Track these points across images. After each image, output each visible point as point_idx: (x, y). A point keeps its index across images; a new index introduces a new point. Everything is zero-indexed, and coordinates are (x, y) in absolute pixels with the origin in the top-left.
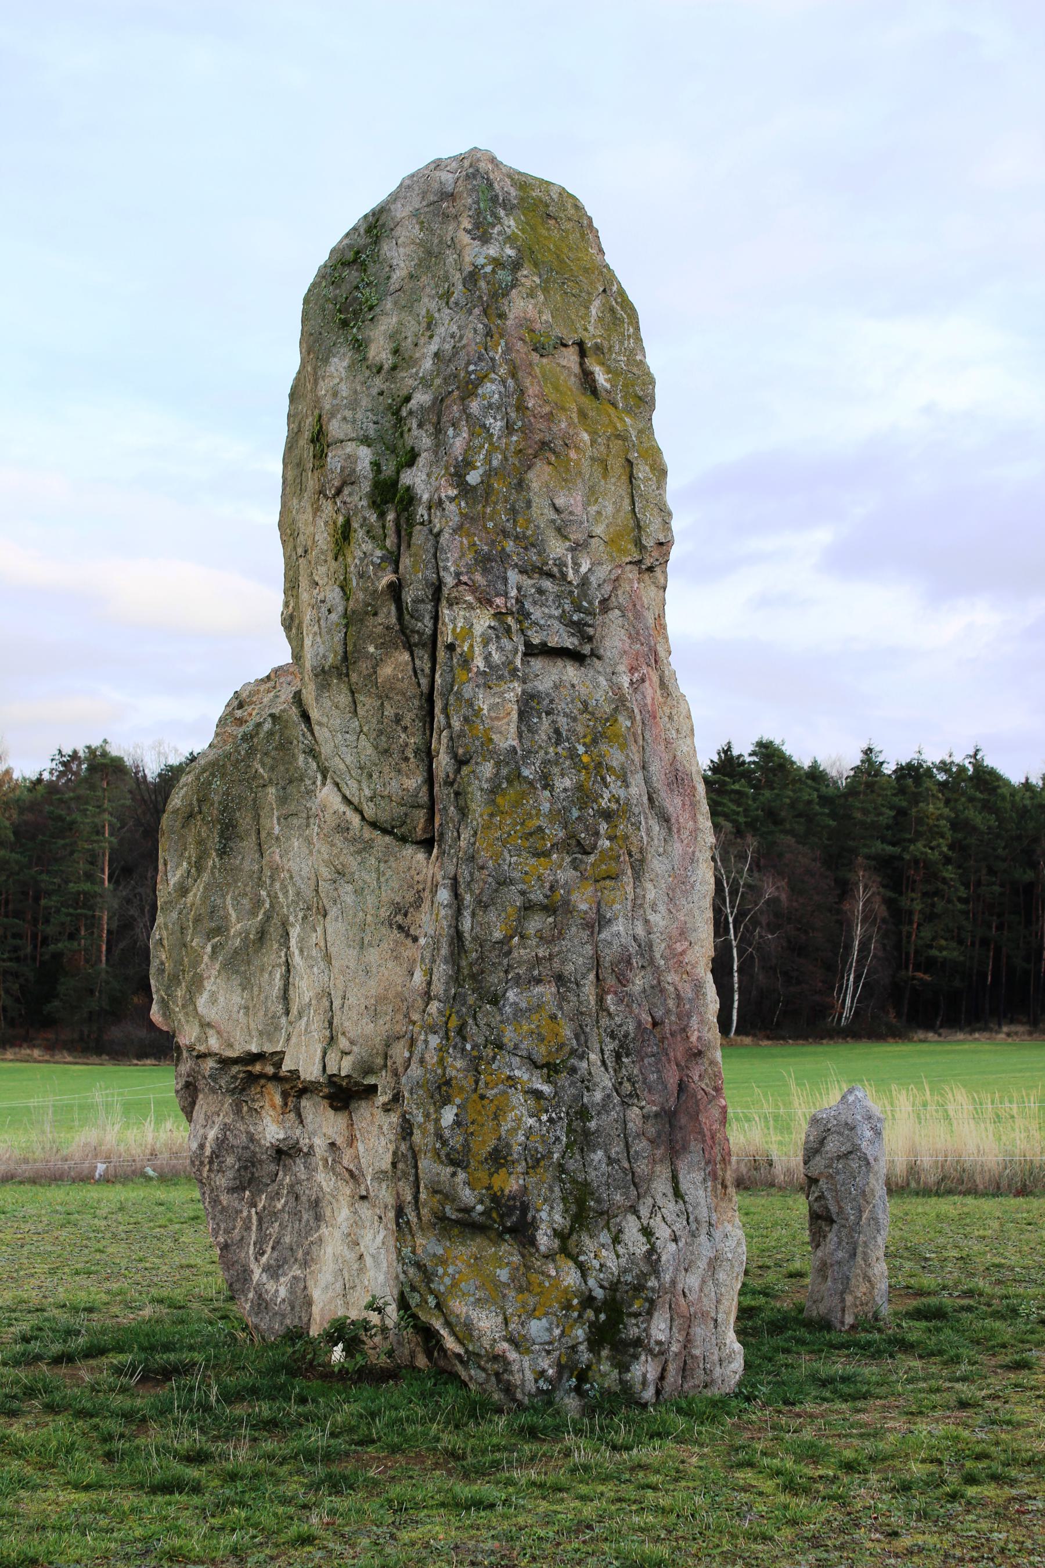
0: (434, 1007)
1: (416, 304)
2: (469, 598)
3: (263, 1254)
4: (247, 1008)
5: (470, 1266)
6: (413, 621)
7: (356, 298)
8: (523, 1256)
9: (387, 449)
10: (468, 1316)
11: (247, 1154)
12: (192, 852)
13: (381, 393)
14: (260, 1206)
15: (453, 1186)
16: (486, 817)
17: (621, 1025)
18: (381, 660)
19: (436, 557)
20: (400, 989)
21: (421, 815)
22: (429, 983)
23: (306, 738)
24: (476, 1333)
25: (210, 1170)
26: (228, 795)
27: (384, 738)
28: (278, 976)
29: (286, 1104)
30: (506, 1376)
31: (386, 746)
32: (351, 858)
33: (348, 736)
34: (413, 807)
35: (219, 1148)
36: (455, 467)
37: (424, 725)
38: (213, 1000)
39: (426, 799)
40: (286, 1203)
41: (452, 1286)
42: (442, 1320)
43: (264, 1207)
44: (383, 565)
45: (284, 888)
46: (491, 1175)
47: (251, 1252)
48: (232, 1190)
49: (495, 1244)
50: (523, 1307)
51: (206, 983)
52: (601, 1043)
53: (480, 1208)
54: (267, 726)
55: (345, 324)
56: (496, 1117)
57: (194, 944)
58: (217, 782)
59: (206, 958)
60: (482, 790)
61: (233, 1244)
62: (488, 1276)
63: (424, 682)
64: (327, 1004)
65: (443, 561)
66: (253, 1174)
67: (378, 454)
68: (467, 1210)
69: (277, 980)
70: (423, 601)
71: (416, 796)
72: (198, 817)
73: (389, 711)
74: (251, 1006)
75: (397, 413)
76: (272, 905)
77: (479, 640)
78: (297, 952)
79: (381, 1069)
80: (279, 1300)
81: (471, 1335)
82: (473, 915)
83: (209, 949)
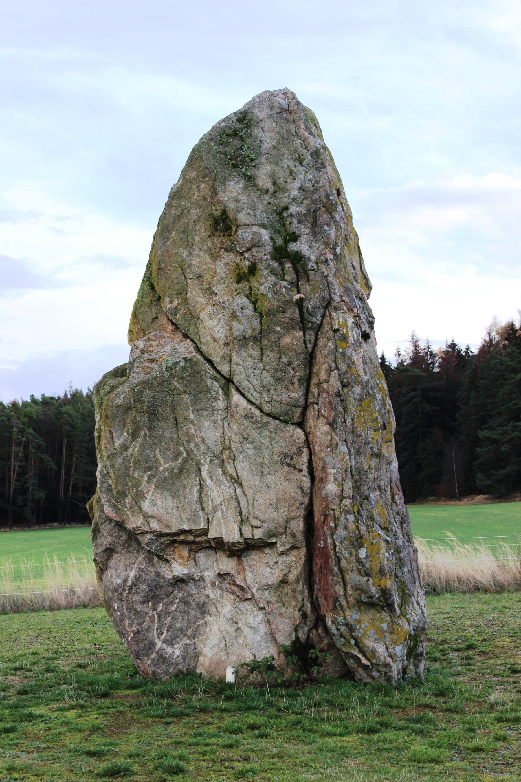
0: (347, 502)
1: (279, 162)
2: (345, 308)
3: (162, 634)
4: (178, 507)
5: (370, 623)
6: (310, 317)
7: (241, 154)
8: (391, 617)
9: (275, 231)
10: (373, 647)
11: (154, 583)
12: (130, 427)
13: (269, 204)
14: (159, 609)
15: (368, 586)
16: (358, 412)
17: (400, 510)
18: (284, 334)
19: (328, 287)
20: (293, 495)
21: (299, 411)
22: (342, 491)
23: (210, 371)
24: (377, 655)
25: (129, 593)
26: (154, 398)
27: (279, 373)
28: (195, 490)
29: (190, 556)
30: (389, 674)
31: (280, 377)
32: (254, 431)
33: (255, 371)
34: (294, 406)
35: (136, 581)
36: (333, 245)
37: (305, 367)
38: (154, 503)
39: (303, 403)
40: (178, 607)
41: (364, 633)
42: (357, 650)
43: (162, 610)
44: (292, 288)
45: (197, 446)
46: (380, 580)
47: (155, 633)
48: (142, 603)
49: (379, 612)
50: (392, 641)
51: (146, 495)
52: (394, 517)
53: (377, 595)
54: (182, 364)
55: (235, 166)
56: (377, 553)
57: (135, 475)
58: (147, 392)
59: (144, 483)
60: (355, 399)
61: (142, 630)
62: (378, 627)
63: (310, 347)
64: (236, 504)
65: (333, 289)
66: (155, 593)
67: (272, 234)
68: (372, 597)
69: (195, 493)
70: (319, 308)
71: (298, 401)
72: (134, 410)
73: (284, 360)
74: (180, 506)
75: (280, 214)
76: (188, 454)
77: (350, 328)
78: (208, 479)
79: (281, 535)
80: (175, 656)
81: (375, 656)
82: (355, 458)
83: (146, 478)
